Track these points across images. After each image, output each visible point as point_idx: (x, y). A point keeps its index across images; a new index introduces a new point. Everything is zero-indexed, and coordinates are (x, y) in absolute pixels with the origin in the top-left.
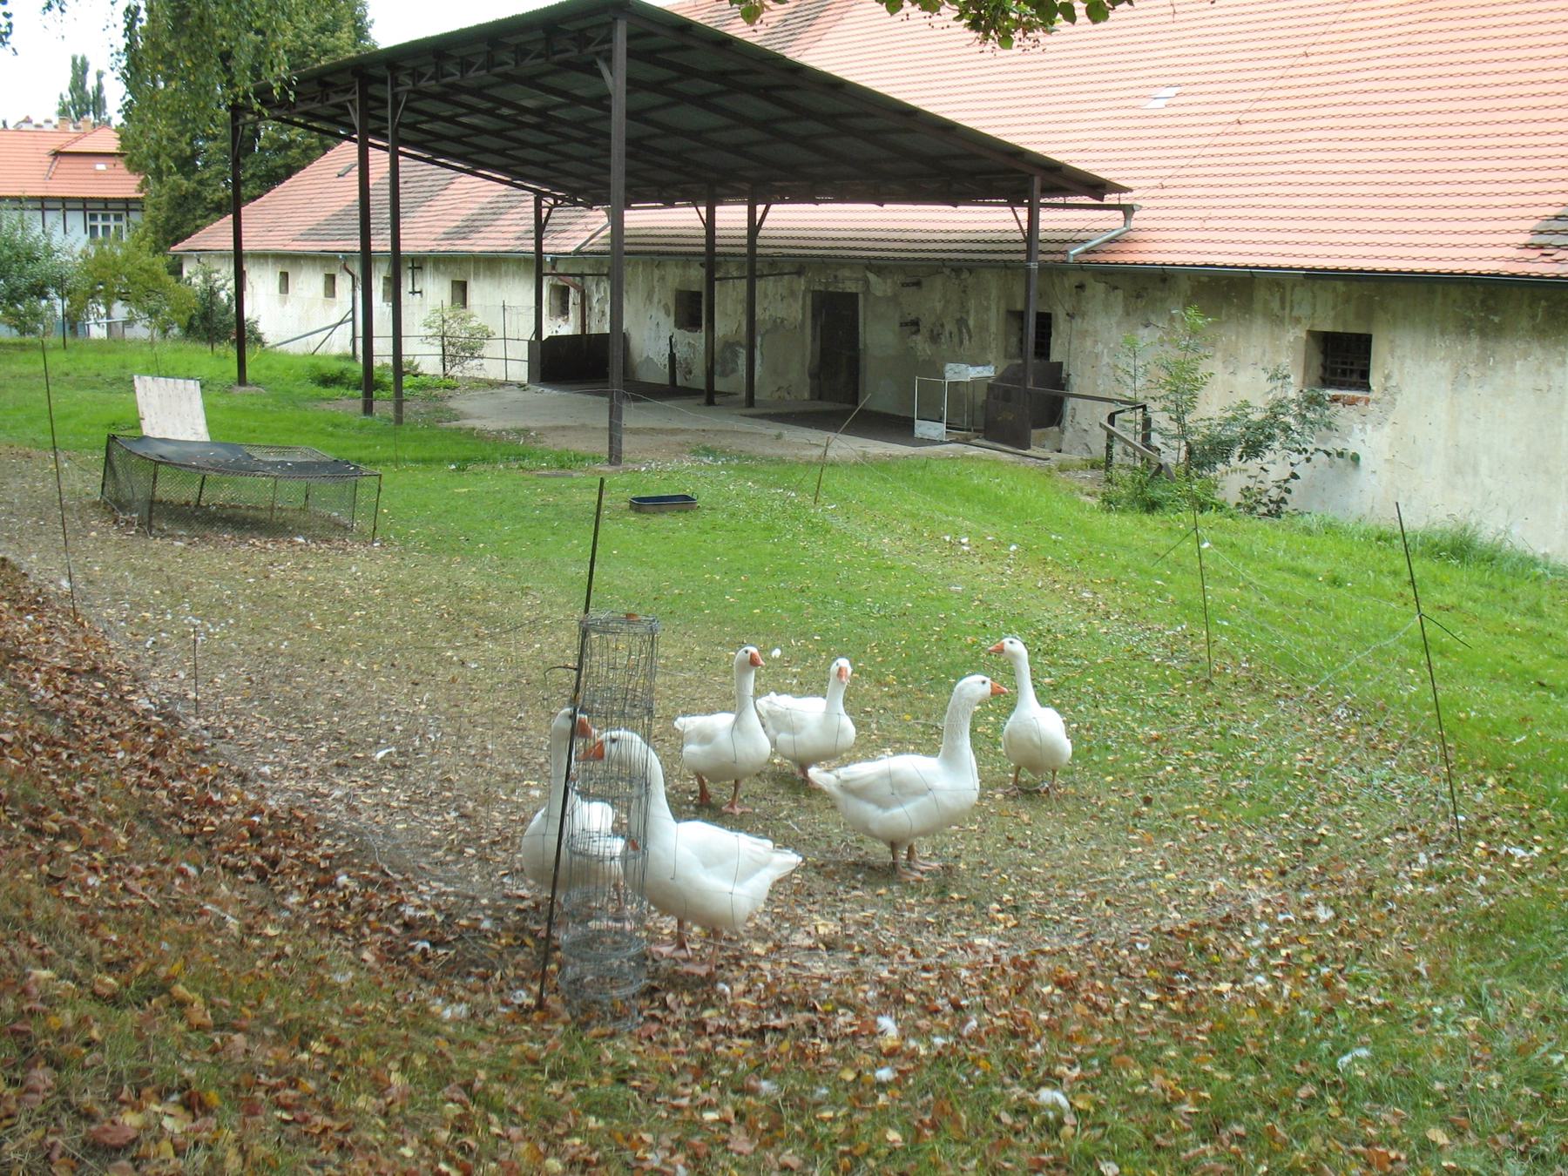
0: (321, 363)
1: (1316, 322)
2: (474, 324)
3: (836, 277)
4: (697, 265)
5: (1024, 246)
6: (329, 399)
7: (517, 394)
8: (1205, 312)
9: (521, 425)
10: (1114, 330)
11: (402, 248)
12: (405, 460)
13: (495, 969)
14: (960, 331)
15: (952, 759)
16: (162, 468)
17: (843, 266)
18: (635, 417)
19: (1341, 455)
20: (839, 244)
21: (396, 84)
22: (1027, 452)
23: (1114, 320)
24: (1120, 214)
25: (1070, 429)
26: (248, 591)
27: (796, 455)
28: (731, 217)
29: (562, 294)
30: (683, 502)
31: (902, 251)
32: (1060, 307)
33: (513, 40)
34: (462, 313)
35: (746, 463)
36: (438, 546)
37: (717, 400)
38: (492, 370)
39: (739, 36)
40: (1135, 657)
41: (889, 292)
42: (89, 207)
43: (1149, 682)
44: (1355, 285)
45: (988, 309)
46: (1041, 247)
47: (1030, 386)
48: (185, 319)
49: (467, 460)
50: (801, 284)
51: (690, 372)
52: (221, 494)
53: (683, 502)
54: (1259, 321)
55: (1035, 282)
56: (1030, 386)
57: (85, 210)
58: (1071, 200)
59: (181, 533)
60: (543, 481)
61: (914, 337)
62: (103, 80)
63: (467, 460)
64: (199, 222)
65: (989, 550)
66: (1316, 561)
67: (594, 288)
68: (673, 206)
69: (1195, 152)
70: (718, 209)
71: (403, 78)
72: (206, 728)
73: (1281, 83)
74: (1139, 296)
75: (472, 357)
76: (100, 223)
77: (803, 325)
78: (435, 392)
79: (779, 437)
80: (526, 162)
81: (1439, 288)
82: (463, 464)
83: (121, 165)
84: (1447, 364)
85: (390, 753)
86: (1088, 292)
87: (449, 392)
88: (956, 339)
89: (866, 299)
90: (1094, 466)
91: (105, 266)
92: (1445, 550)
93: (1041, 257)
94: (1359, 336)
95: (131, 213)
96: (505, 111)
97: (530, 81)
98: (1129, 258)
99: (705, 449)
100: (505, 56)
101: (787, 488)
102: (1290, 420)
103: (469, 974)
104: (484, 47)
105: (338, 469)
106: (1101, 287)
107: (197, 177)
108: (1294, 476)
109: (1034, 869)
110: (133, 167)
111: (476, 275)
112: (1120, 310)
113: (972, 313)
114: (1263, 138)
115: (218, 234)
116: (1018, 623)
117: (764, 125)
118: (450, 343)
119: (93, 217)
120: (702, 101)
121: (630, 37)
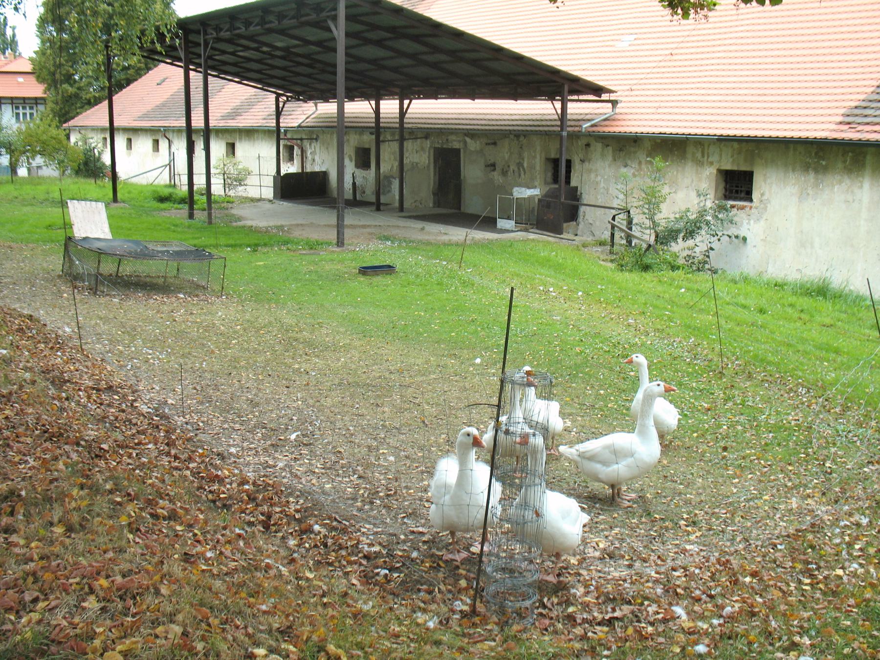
0: (159, 189)
1: (722, 164)
2: (240, 167)
3: (447, 140)
4: (368, 133)
5: (559, 123)
6: (165, 209)
7: (268, 206)
8: (665, 159)
9: (279, 224)
10: (607, 169)
11: (193, 125)
12: (220, 245)
13: (434, 586)
14: (519, 169)
15: (643, 434)
16: (103, 256)
17: (452, 133)
18: (351, 218)
19: (737, 237)
20: (450, 121)
21: (206, 33)
22: (561, 236)
23: (607, 163)
24: (610, 105)
25: (582, 223)
26: (168, 330)
27: (435, 239)
28: (390, 107)
29: (290, 149)
30: (388, 269)
31: (486, 125)
32: (576, 156)
33: (276, 9)
34: (234, 161)
35: (414, 246)
36: (258, 297)
37: (382, 208)
38: (253, 192)
39: (409, 8)
40: (675, 359)
41: (478, 148)
42: (16, 102)
43: (689, 374)
44: (744, 144)
45: (535, 157)
46: (569, 123)
47: (562, 200)
48: (75, 165)
49: (257, 245)
50: (428, 144)
51: (364, 192)
52: (128, 269)
53: (388, 269)
54: (690, 164)
55: (565, 143)
56: (562, 200)
57: (12, 104)
58: (581, 97)
59: (114, 293)
60: (304, 257)
61: (493, 173)
62: (15, 31)
63: (257, 245)
64: (78, 111)
65: (567, 294)
66: (746, 299)
67: (308, 146)
68: (353, 100)
69: (648, 71)
70: (381, 102)
71: (210, 31)
72: (187, 423)
73: (694, 33)
74: (621, 150)
75: (240, 185)
76: (21, 111)
77: (428, 166)
78: (223, 205)
79: (423, 229)
80: (272, 77)
81: (792, 146)
82: (255, 247)
83: (32, 79)
84: (797, 187)
85: (298, 435)
86: (592, 148)
87: (230, 205)
88: (517, 174)
89: (465, 152)
90: (602, 244)
91: (31, 136)
92: (814, 291)
93: (569, 129)
94: (745, 172)
95: (38, 106)
96: (265, 49)
97: (282, 32)
98: (617, 129)
99: (384, 236)
100: (271, 18)
101: (441, 260)
102: (709, 218)
103: (419, 590)
104: (260, 13)
105: (199, 254)
106: (599, 146)
107: (77, 85)
108: (712, 249)
109: (688, 496)
110: (40, 80)
111: (240, 139)
112: (610, 158)
113: (526, 160)
114: (686, 63)
115: (97, 116)
116: (642, 348)
117: (413, 56)
118: (228, 178)
119: (17, 108)
120: (379, 43)
121: (347, 7)
